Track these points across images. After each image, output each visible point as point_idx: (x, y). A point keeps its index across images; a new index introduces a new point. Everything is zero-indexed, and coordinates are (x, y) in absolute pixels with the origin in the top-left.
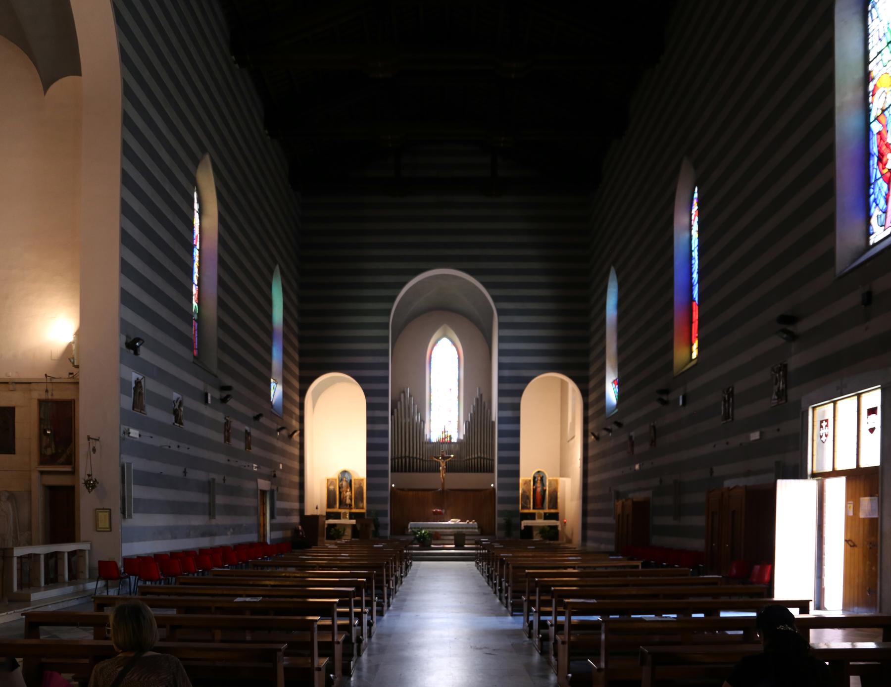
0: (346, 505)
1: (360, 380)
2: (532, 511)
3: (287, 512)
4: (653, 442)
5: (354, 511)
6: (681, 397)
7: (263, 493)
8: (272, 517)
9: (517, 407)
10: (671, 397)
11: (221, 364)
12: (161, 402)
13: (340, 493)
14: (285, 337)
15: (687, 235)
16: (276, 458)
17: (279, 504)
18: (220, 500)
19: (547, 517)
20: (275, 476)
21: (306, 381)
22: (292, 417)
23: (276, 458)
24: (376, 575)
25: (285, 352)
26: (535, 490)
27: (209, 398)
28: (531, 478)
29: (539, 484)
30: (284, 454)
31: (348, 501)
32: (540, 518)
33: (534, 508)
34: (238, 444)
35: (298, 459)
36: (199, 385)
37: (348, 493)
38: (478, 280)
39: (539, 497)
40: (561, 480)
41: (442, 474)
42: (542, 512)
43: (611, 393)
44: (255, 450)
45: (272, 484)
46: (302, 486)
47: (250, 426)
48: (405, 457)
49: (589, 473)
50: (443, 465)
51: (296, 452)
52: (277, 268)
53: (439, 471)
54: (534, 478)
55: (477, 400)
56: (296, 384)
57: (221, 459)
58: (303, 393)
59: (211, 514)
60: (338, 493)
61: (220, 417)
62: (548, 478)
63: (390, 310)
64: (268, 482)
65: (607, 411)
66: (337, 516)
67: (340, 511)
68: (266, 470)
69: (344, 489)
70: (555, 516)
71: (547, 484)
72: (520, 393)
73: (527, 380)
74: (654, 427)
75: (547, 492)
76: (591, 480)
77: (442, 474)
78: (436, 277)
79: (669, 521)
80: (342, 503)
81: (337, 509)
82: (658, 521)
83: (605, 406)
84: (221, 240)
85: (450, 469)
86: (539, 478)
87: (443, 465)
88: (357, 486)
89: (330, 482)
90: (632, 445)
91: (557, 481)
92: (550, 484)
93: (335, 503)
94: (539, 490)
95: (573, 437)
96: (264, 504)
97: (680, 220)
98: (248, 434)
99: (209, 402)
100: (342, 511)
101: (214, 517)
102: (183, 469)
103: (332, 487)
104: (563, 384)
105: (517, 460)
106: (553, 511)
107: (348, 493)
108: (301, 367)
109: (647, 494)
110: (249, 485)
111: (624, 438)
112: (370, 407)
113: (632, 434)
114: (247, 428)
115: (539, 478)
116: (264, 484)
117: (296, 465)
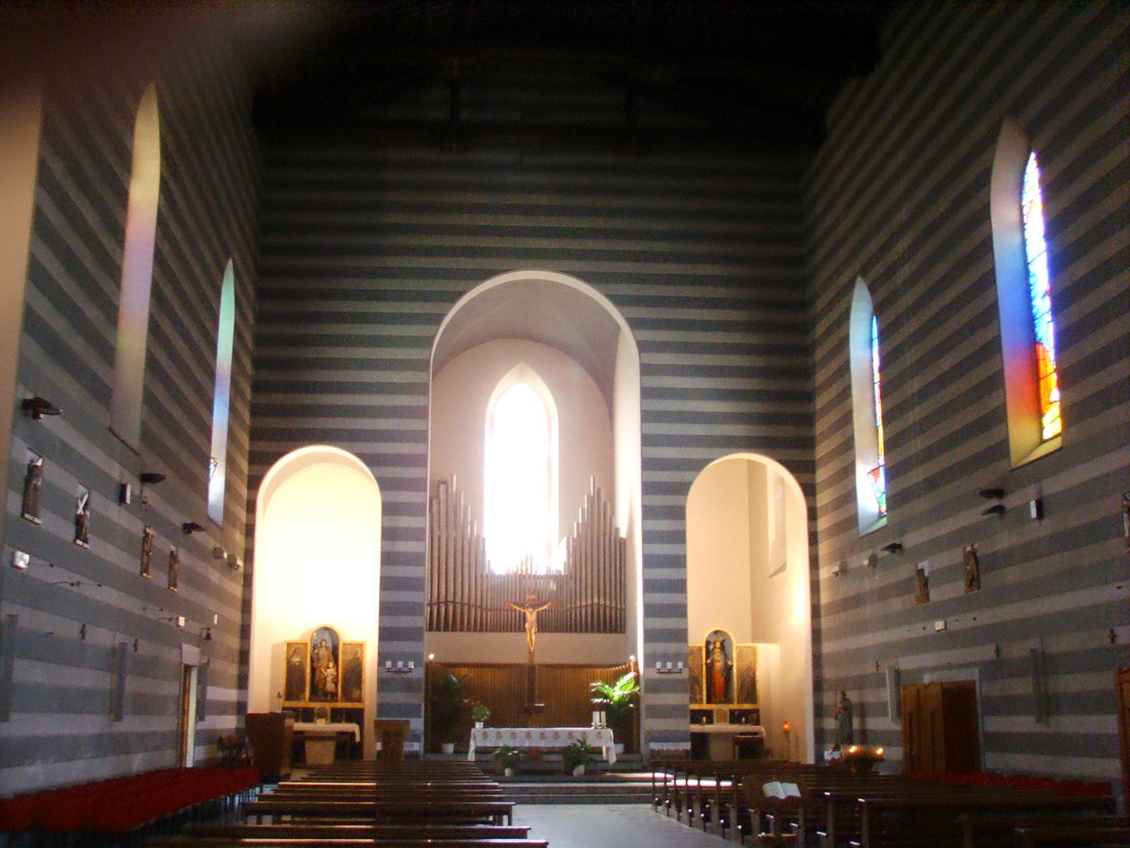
0: (326, 694)
1: (371, 460)
2: (705, 706)
3: (222, 708)
4: (973, 582)
5: (340, 705)
6: (1033, 504)
7: (188, 668)
8: (200, 716)
9: (678, 513)
10: (1010, 502)
11: (147, 435)
12: (946, 575)
13: (313, 670)
14: (235, 385)
15: (1018, 239)
16: (210, 603)
17: (214, 693)
18: (132, 685)
19: (735, 717)
20: (208, 637)
21: (262, 460)
22: (235, 526)
23: (210, 603)
24: (837, 800)
25: (233, 410)
26: (710, 668)
27: (128, 494)
28: (704, 645)
29: (718, 656)
30: (221, 595)
31: (330, 686)
32: (720, 719)
33: (708, 702)
34: (158, 577)
35: (239, 604)
36: (116, 471)
37: (331, 671)
38: (600, 291)
39: (719, 680)
40: (762, 648)
41: (532, 634)
42: (726, 708)
43: (871, 494)
44: (181, 590)
45: (202, 653)
46: (244, 657)
47: (177, 544)
48: (462, 605)
49: (824, 636)
50: (531, 616)
51: (237, 590)
52: (230, 262)
53: (524, 630)
54: (708, 643)
55: (591, 500)
56: (244, 465)
57: (133, 605)
58: (254, 483)
59: (116, 711)
60: (308, 670)
61: (137, 527)
62: (738, 644)
63: (433, 338)
64: (196, 650)
65: (862, 523)
66: (307, 715)
67: (312, 705)
68: (196, 628)
69: (324, 662)
70: (752, 716)
71: (735, 655)
72: (683, 489)
73: (698, 465)
74: (973, 552)
75: (735, 671)
76: (827, 647)
77: (532, 634)
78: (526, 283)
79: (1024, 724)
80: (318, 691)
81: (305, 702)
82: (992, 724)
83: (856, 514)
84: (161, 222)
85: (543, 626)
86: (719, 642)
87: (531, 616)
88: (350, 657)
89: (293, 648)
90: (925, 584)
91: (754, 652)
92: (740, 655)
93: (303, 691)
94: (719, 665)
95: (783, 568)
96: (185, 691)
97: (1002, 215)
98: (173, 556)
99: (128, 501)
100: (317, 705)
101: (119, 718)
102: (993, 647)
103: (296, 659)
104: (755, 473)
105: (680, 611)
106: (747, 706)
107: (331, 671)
108: (255, 434)
109: (973, 674)
110: (170, 655)
111: (904, 571)
112: (389, 509)
113: (924, 565)
114: (173, 548)
115: (719, 642)
116: (191, 654)
117: (236, 617)
